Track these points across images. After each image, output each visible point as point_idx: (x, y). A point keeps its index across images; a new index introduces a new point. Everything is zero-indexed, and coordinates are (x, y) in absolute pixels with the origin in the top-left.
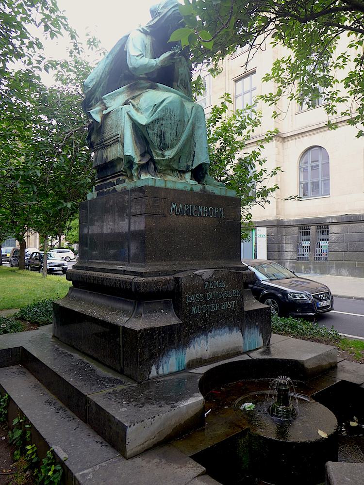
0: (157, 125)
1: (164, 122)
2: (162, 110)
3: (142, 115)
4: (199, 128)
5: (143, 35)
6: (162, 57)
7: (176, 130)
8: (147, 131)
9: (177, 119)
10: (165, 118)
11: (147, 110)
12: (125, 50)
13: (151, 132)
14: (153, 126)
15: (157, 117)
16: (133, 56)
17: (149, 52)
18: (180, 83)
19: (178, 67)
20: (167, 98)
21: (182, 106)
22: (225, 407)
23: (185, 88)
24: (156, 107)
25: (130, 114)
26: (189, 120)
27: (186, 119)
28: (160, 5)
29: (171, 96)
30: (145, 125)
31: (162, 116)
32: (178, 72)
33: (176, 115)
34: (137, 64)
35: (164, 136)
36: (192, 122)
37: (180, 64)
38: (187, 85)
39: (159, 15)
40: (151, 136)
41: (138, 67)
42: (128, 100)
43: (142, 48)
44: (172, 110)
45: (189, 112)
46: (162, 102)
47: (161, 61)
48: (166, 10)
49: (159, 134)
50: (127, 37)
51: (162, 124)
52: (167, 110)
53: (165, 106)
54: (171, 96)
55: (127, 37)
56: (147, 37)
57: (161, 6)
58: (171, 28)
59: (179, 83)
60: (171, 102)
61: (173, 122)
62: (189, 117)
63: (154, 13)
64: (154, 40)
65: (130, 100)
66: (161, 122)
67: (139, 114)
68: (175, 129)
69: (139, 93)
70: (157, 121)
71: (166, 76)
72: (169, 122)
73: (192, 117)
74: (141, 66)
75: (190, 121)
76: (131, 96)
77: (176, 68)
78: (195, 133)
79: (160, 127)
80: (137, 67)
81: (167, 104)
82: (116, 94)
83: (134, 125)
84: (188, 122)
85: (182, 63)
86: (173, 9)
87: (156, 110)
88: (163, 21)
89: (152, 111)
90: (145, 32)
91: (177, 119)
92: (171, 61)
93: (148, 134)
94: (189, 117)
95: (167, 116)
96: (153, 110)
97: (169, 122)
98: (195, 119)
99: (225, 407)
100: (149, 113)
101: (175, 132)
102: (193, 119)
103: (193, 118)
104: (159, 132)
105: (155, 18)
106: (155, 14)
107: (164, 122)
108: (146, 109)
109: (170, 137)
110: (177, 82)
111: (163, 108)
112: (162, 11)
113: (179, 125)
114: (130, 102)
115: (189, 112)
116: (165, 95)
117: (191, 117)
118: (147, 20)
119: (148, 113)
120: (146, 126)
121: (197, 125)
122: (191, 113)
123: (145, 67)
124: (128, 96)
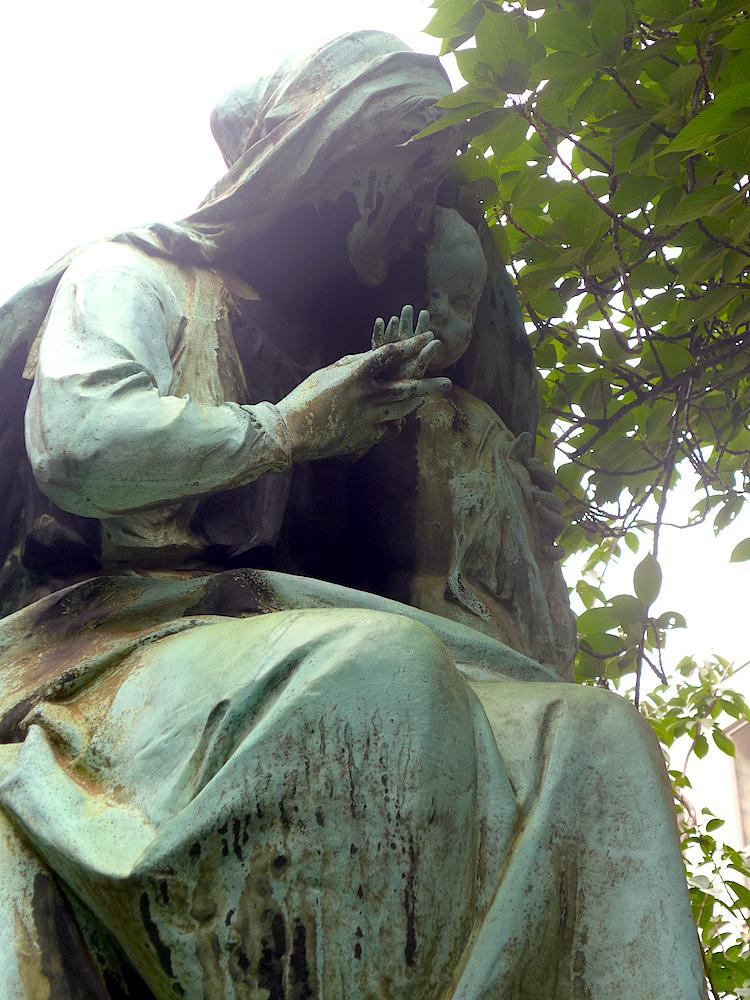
0: (235, 874)
1: (294, 845)
2: (283, 742)
3: (121, 811)
4: (615, 873)
5: (158, 272)
6: (301, 396)
7: (409, 899)
8: (152, 929)
9: (412, 802)
10: (307, 806)
11: (157, 760)
12: (26, 375)
13: (188, 937)
14: (205, 886)
15: (232, 798)
16: (62, 382)
17: (212, 372)
18: (468, 574)
19: (444, 464)
20: (316, 644)
21: (451, 702)
22: (624, 653)
23: (508, 605)
24: (227, 723)
25: (19, 808)
26: (521, 815)
27: (496, 808)
28: (278, 77)
29: (347, 629)
30: (134, 882)
31: (276, 792)
32: (447, 498)
33: (393, 769)
34: (88, 435)
35: (299, 962)
36: (553, 828)
37: (457, 445)
38: (522, 585)
39: (275, 138)
40: (186, 966)
41: (97, 455)
42: (24, 707)
43: (143, 340)
44: (357, 731)
45: (518, 748)
46: (276, 680)
47: (294, 416)
48: (324, 96)
49: (255, 953)
50: (45, 293)
51: (281, 862)
52: (314, 742)
53: (295, 710)
54: (347, 629)
55: (45, 293)
56: (191, 278)
57: (284, 85)
58: (364, 212)
59: (455, 572)
60: (349, 672)
61: (374, 833)
62: (524, 784)
63: (231, 130)
64: (251, 296)
65: (43, 708)
66: (274, 841)
67: (98, 805)
68: (394, 898)
69: (119, 644)
70: (231, 834)
71: (344, 519)
72: (338, 833)
73: (549, 783)
74: (118, 442)
75: (535, 822)
76: (52, 678)
77: (425, 471)
78: (592, 918)
79: (264, 891)
80: (82, 449)
81: (315, 686)
82: (221, 759)
83: (51, 892)
84: (517, 827)
85: (476, 437)
86: (370, 89)
87: (228, 745)
88: (302, 168)
89: (197, 760)
90: (174, 250)
91: (412, 802)
92: (371, 413)
93: (164, 954)
94: (524, 784)
95: (319, 784)
96: (203, 748)
97: (338, 833)
98: (580, 799)
99: (624, 653)
100: (173, 781)
101: (400, 921)
102: (555, 805)
103: (559, 790)
104: (257, 932)
105: (248, 162)
106: (245, 140)
107: (294, 845)
108: (155, 753)
109: (355, 966)
110: (446, 572)
111: (281, 722)
112: (289, 109)
113: (427, 855)
114: (38, 719)
115: (518, 748)
116: (294, 628)
117: (537, 787)
118: (190, 180)
119: (166, 788)
120: (148, 889)
121: (603, 848)
122: (541, 755)
123: (152, 451)
124: (28, 679)
